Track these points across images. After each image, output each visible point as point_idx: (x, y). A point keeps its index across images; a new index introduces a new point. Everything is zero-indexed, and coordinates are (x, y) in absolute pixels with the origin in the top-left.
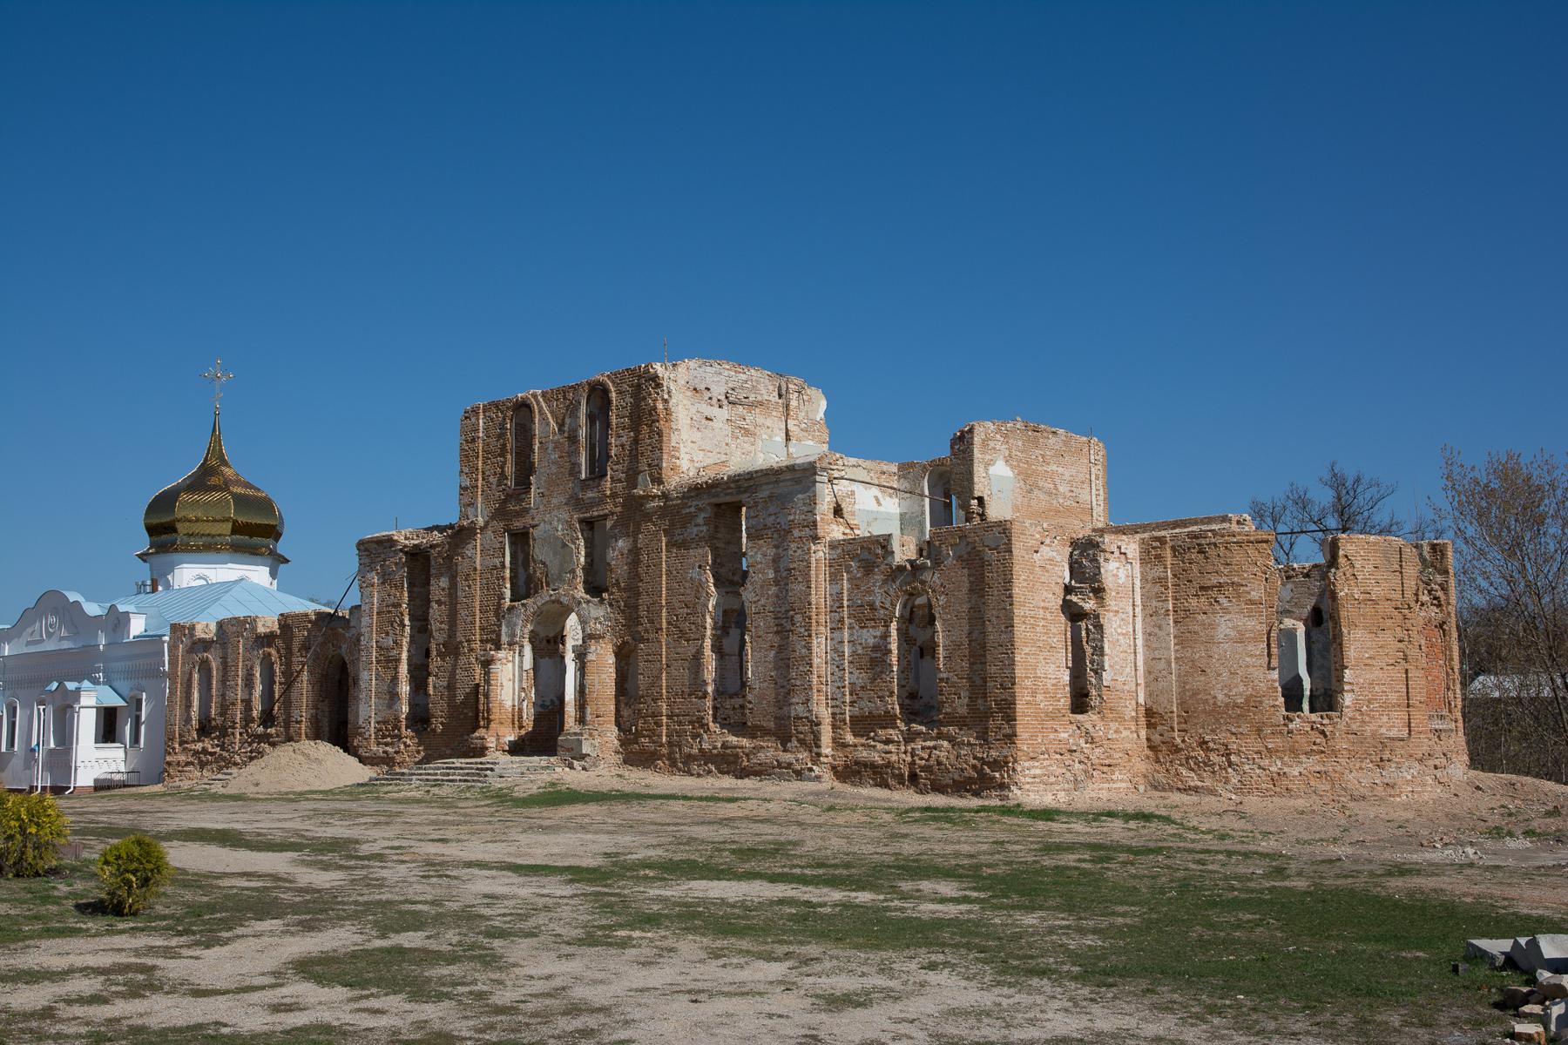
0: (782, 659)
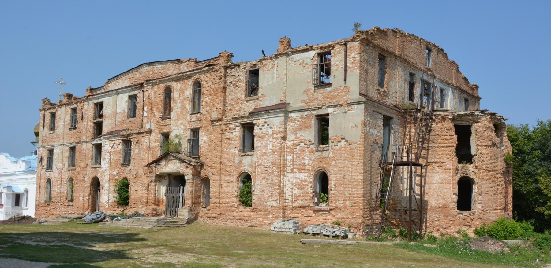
0: (267, 184)
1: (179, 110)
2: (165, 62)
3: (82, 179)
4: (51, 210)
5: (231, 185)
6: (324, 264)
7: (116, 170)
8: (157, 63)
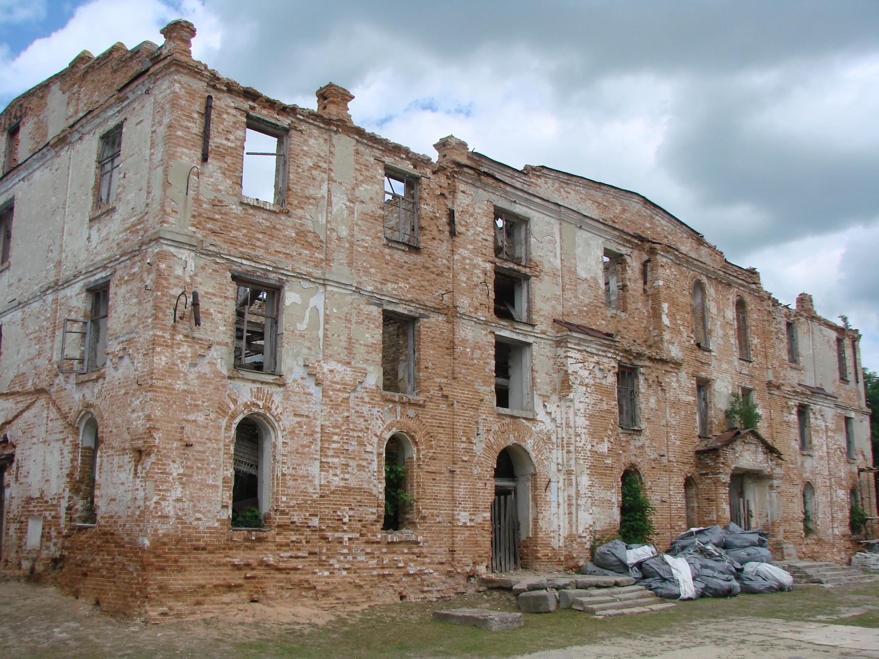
1: (720, 341)
2: (676, 222)
3: (463, 445)
4: (282, 565)
5: (795, 500)
6: (159, 469)
7: (606, 439)
8: (661, 212)
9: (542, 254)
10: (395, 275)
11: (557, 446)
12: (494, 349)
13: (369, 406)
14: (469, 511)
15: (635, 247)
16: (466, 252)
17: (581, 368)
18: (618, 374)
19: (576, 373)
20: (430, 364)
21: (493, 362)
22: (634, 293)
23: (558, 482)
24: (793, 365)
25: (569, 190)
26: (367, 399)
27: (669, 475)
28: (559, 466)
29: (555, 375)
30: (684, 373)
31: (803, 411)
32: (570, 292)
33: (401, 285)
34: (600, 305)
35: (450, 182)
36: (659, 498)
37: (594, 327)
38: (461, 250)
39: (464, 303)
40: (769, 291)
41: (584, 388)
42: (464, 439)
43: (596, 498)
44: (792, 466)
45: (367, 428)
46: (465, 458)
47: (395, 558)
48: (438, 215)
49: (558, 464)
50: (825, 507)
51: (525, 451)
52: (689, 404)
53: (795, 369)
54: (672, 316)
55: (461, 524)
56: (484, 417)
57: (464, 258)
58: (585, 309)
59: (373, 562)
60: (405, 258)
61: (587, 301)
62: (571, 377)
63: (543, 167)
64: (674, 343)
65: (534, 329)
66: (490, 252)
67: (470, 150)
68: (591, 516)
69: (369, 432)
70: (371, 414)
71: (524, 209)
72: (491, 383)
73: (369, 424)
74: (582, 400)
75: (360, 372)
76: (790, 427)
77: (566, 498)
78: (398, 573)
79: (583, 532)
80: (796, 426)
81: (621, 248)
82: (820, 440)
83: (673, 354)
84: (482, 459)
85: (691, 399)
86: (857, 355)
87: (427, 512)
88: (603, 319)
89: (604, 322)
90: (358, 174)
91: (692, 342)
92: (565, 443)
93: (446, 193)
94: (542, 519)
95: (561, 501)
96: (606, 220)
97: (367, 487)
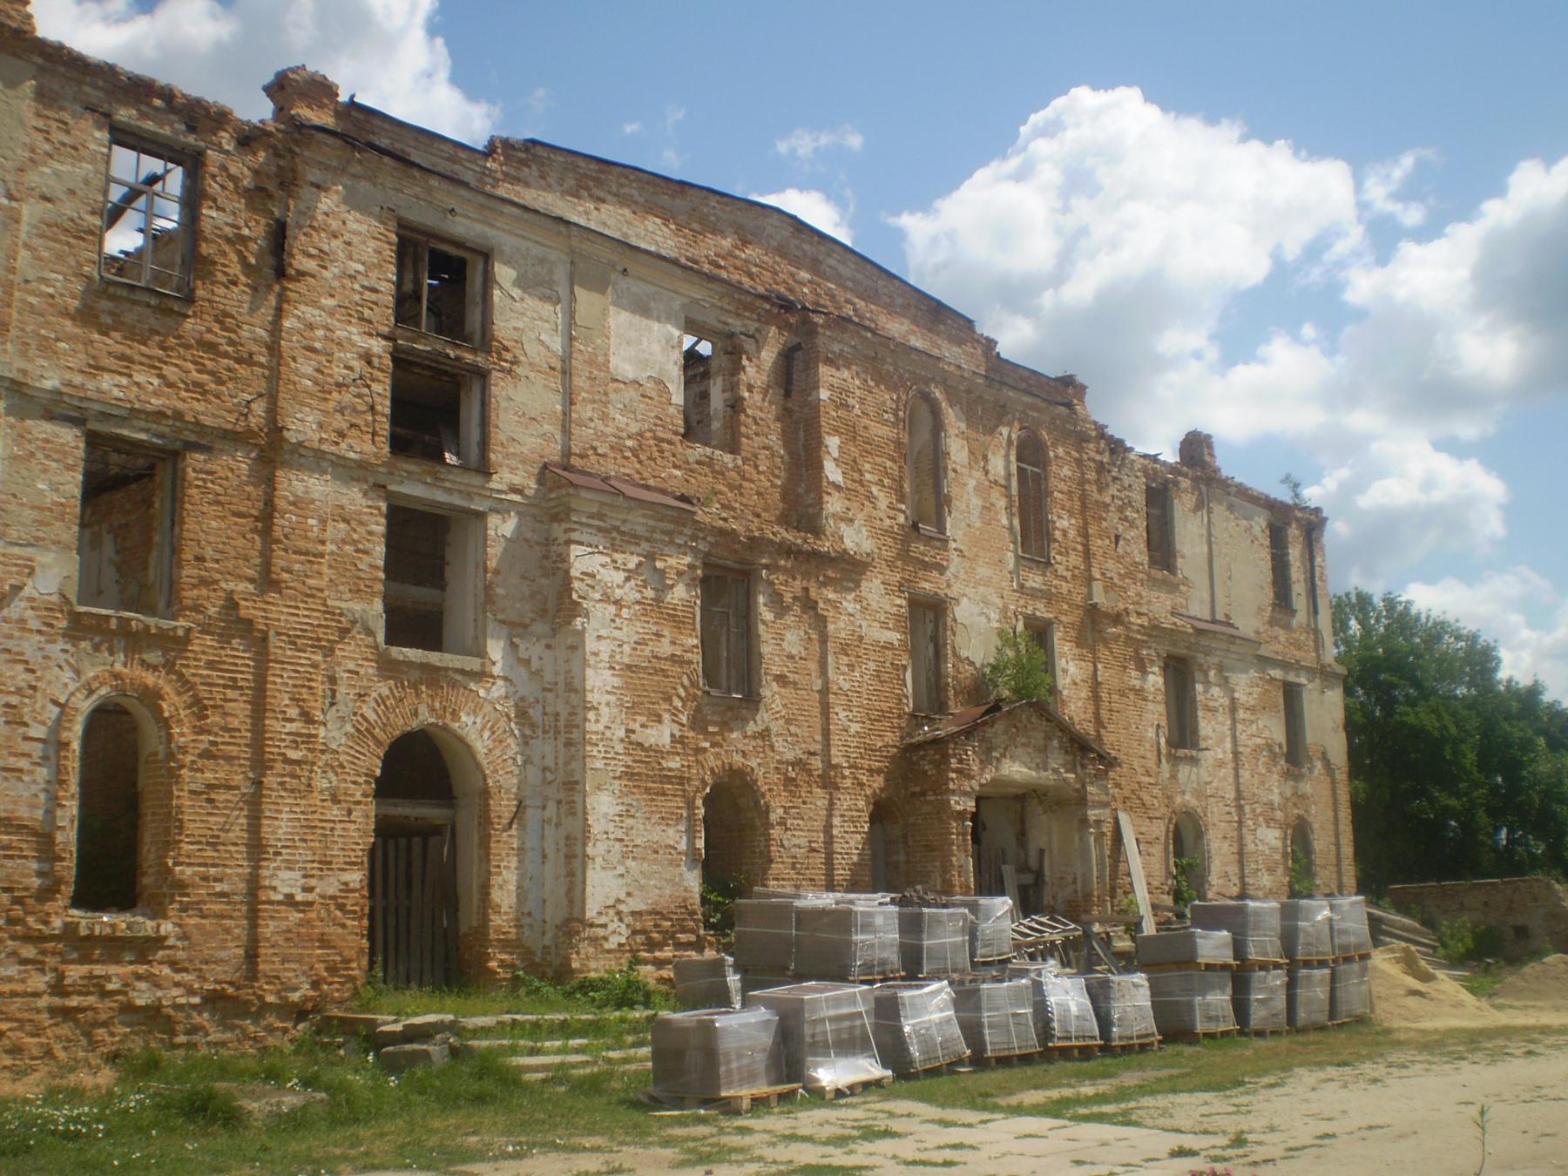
7: (666, 717)
9: (520, 325)
10: (123, 357)
11: (544, 732)
12: (383, 521)
13: (38, 637)
14: (300, 869)
15: (766, 319)
16: (316, 312)
17: (603, 566)
18: (704, 581)
19: (593, 576)
20: (209, 552)
21: (380, 550)
22: (759, 414)
23: (544, 808)
24: (1159, 574)
25: (601, 194)
26: (34, 624)
27: (831, 794)
28: (548, 774)
29: (544, 581)
30: (877, 582)
31: (1180, 673)
32: (589, 407)
33: (138, 378)
34: (669, 436)
35: (282, 163)
36: (803, 842)
37: (651, 482)
38: (303, 307)
39: (303, 425)
40: (1101, 422)
41: (612, 609)
42: (293, 712)
43: (638, 841)
44: (1147, 779)
45: (34, 688)
46: (294, 755)
47: (97, 973)
48: (246, 232)
49: (544, 769)
50: (1226, 864)
51: (461, 740)
52: (888, 646)
53: (1164, 582)
54: (851, 466)
55: (280, 897)
56: (351, 666)
57: (311, 327)
58: (630, 443)
59: (39, 982)
60: (152, 320)
61: (634, 428)
62: (576, 585)
63: (534, 142)
64: (852, 521)
65: (488, 482)
66: (384, 317)
67: (343, 98)
68: (621, 881)
69: (38, 694)
70: (45, 657)
71: (479, 227)
72: (373, 594)
73: (39, 679)
74: (603, 632)
75: (16, 565)
76: (1145, 699)
77: (562, 843)
78: (105, 1008)
79: (600, 913)
80: (1160, 698)
81: (730, 321)
82: (1218, 728)
83: (849, 544)
84: (342, 758)
85: (894, 637)
86: (1318, 560)
87: (189, 871)
88: (675, 466)
89: (678, 473)
90: (40, 137)
91: (901, 519)
92: (561, 724)
93: (271, 186)
94: (501, 887)
95: (550, 851)
96: (696, 262)
97: (26, 815)
